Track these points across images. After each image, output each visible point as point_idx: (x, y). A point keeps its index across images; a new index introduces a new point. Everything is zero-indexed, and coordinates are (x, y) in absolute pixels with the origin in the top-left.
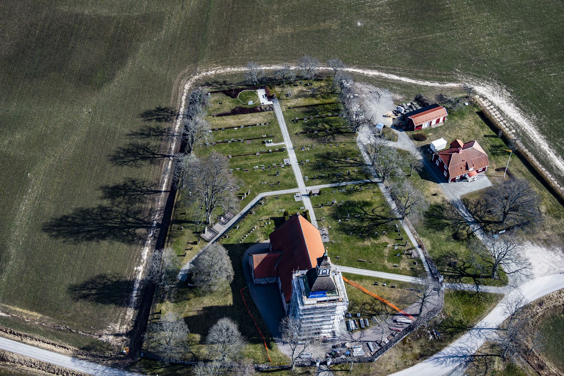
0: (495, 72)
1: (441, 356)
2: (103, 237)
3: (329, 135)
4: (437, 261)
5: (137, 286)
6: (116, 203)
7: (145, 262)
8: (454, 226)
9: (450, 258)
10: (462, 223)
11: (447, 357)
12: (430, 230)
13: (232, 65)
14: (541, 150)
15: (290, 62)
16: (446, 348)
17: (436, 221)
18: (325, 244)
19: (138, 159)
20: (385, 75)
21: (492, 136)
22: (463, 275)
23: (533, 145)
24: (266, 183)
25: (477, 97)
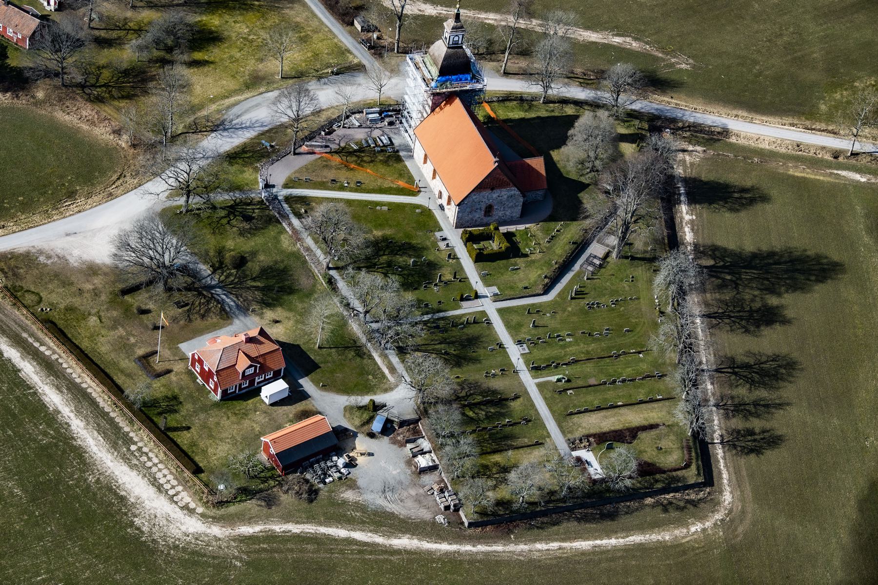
0: (162, 569)
1: (258, 129)
2: (754, 256)
3: (463, 397)
4: (271, 221)
5: (683, 198)
6: (758, 299)
7: (684, 224)
8: (244, 278)
9: (250, 228)
10: (230, 284)
11: (250, 127)
12: (282, 266)
13: (661, 547)
14: (86, 418)
15: (560, 558)
16: (252, 137)
17: (272, 282)
18: (441, 230)
19: (755, 365)
20: (379, 539)
21: (176, 429)
22: (231, 207)
23: (98, 425)
24: (548, 315)
25: (200, 510)
